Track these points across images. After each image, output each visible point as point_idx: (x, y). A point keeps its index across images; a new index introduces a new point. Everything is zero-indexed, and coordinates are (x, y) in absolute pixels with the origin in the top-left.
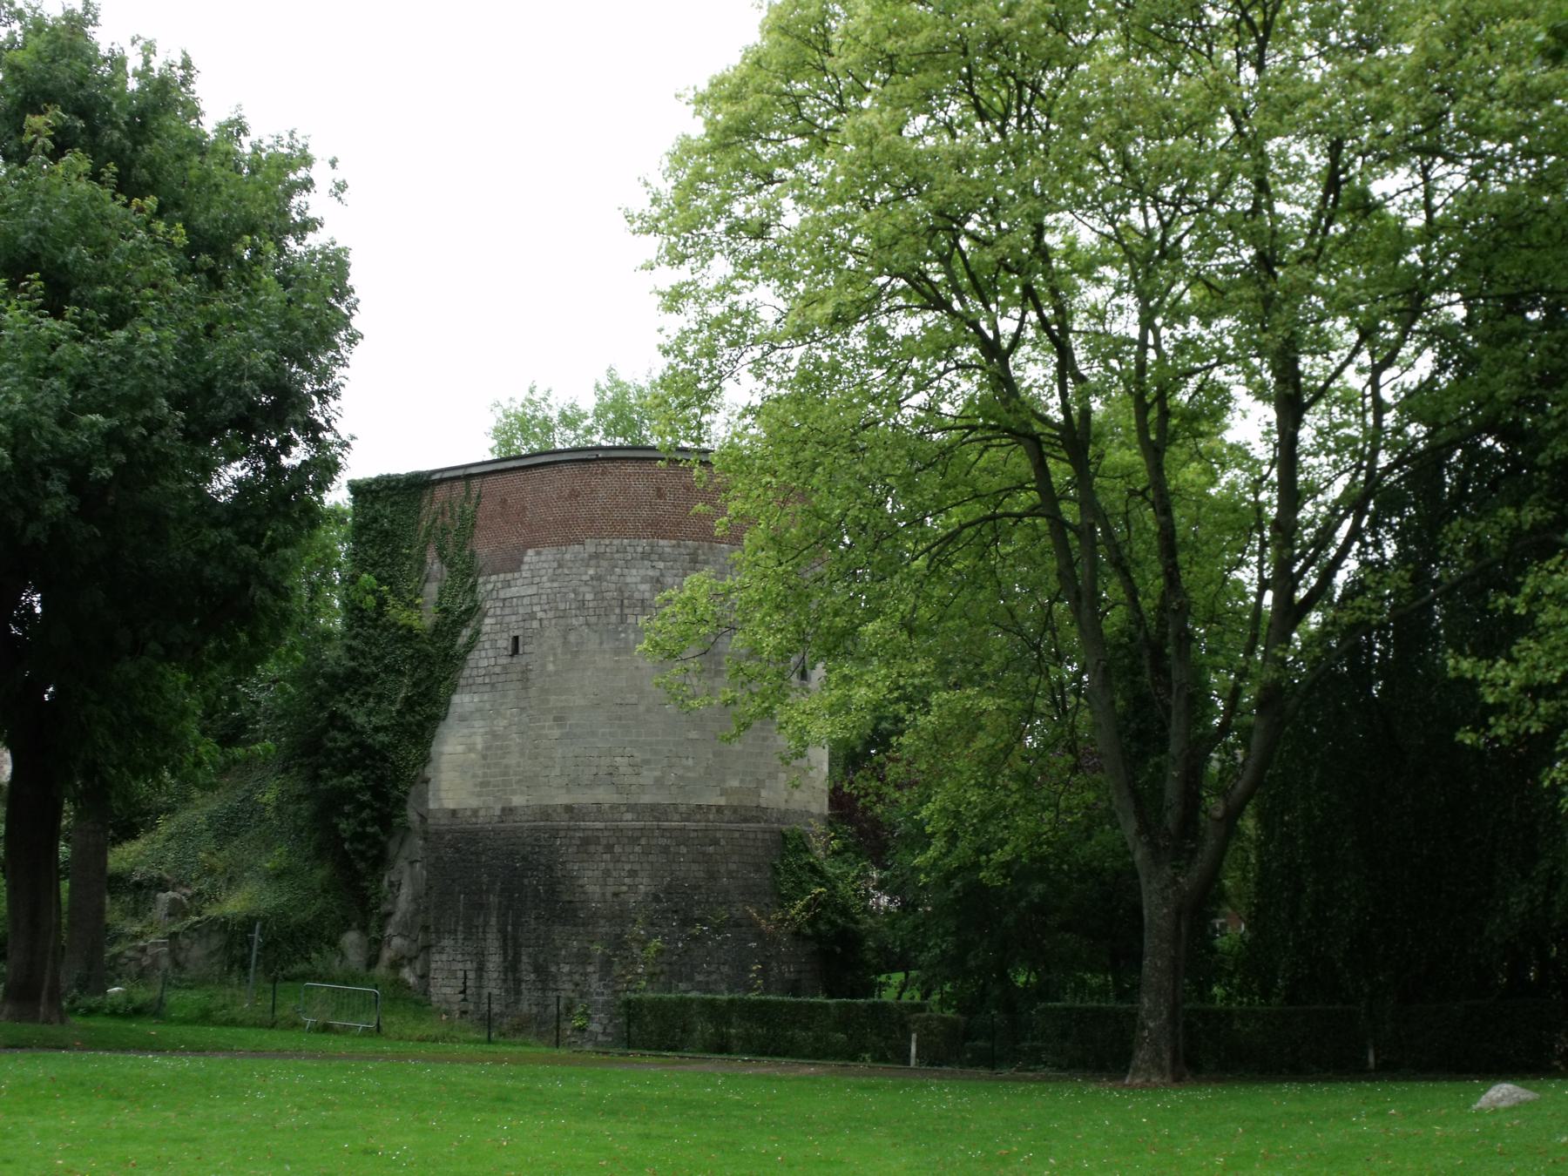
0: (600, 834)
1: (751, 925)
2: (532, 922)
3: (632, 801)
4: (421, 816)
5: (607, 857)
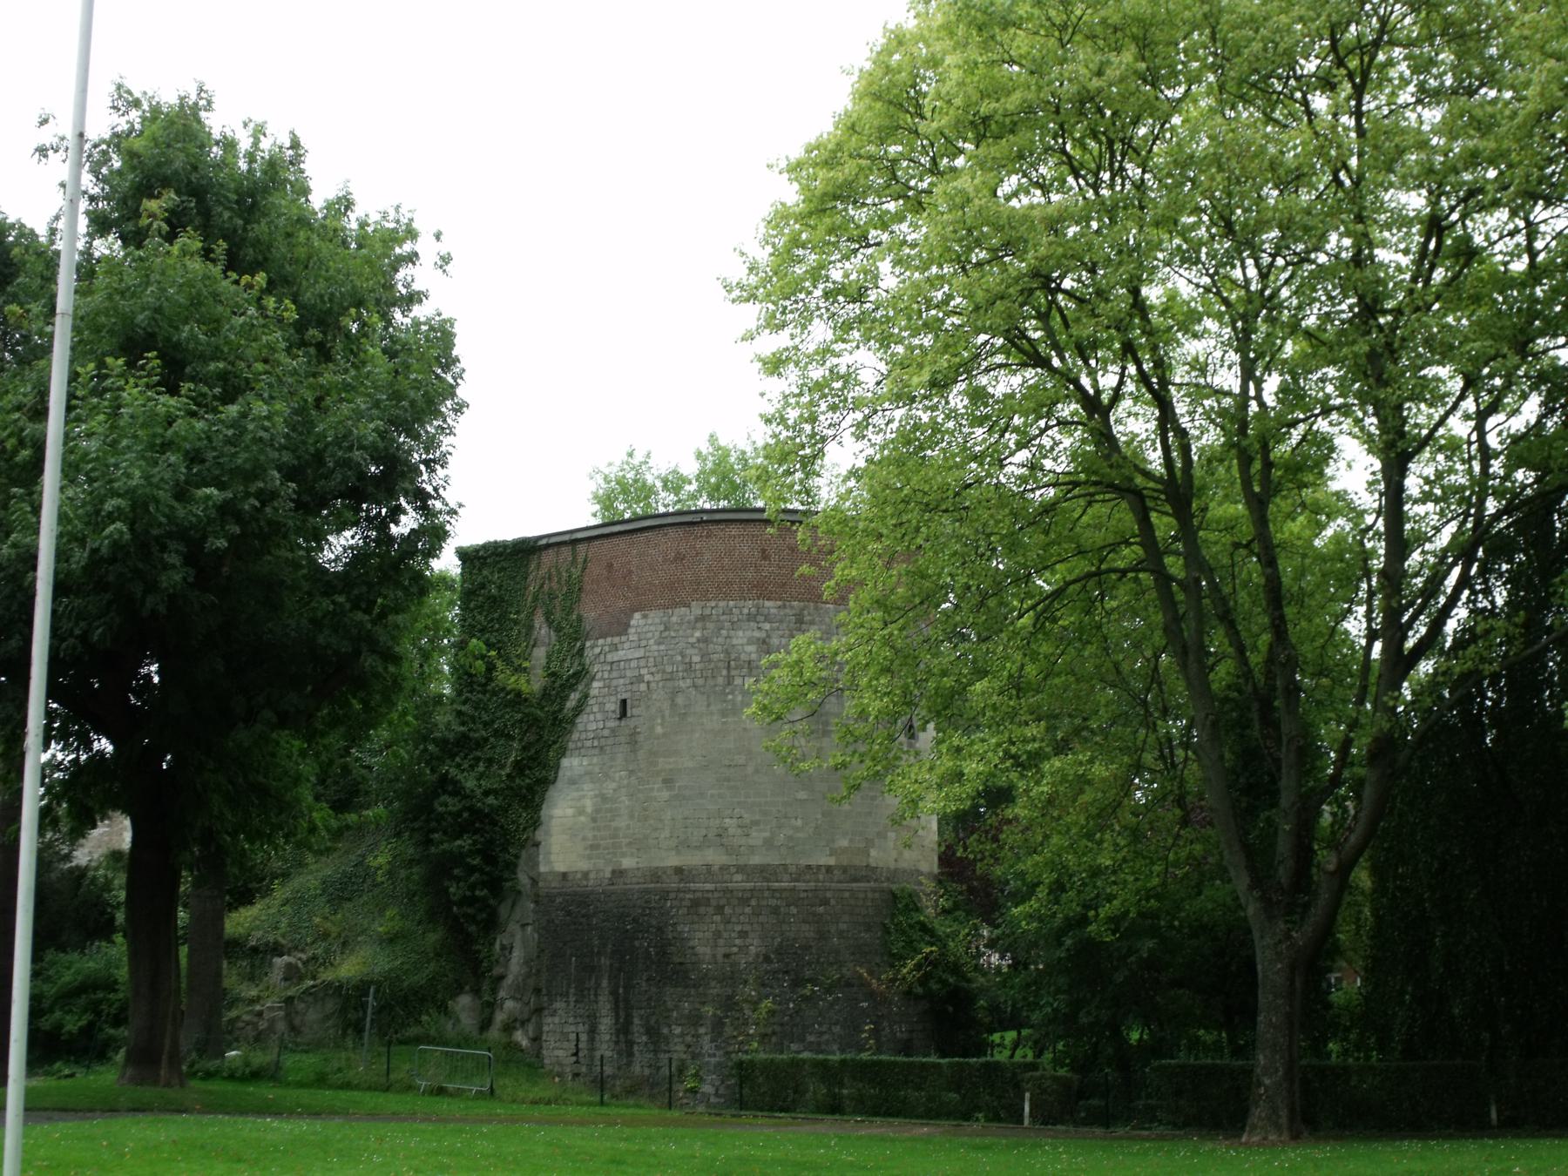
0: (710, 895)
1: (862, 985)
2: (644, 984)
3: (742, 861)
4: (532, 879)
5: (717, 918)
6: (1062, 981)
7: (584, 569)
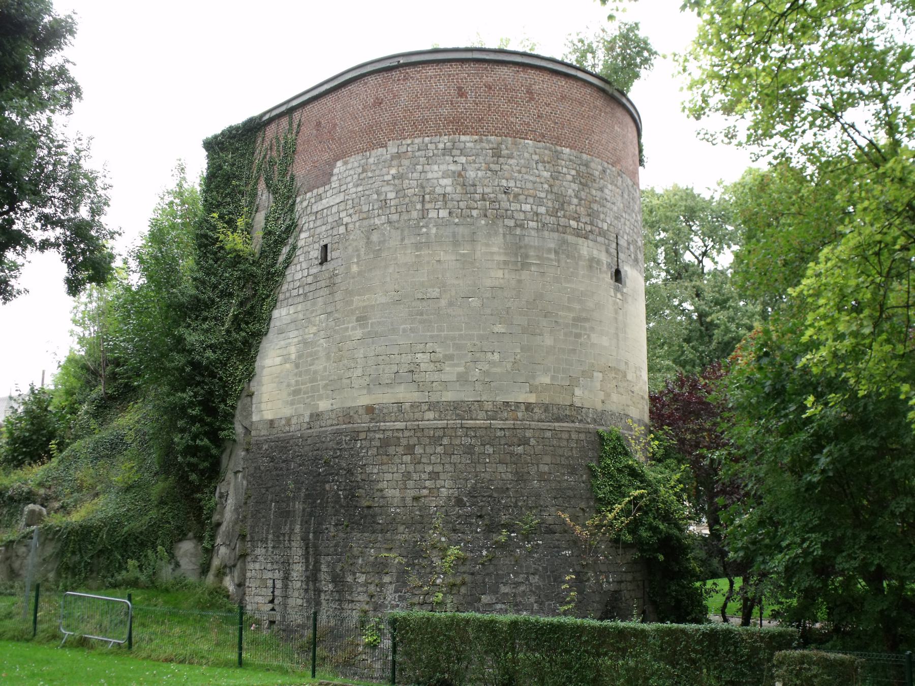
0: (400, 435)
1: (565, 531)
3: (434, 398)
5: (408, 458)
6: (812, 517)
7: (298, 132)
